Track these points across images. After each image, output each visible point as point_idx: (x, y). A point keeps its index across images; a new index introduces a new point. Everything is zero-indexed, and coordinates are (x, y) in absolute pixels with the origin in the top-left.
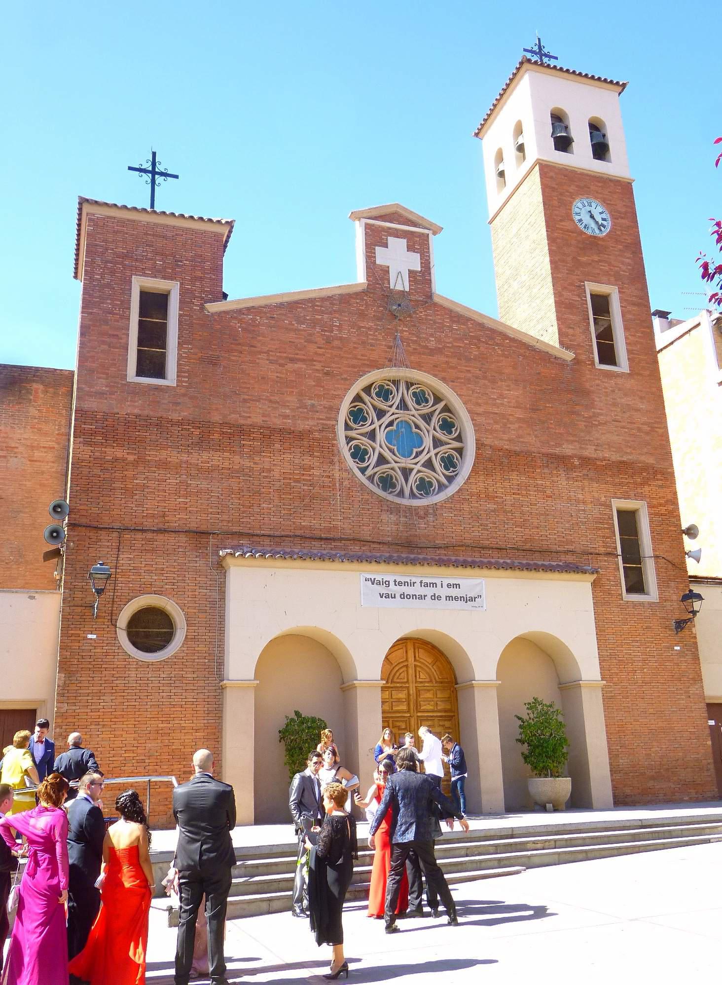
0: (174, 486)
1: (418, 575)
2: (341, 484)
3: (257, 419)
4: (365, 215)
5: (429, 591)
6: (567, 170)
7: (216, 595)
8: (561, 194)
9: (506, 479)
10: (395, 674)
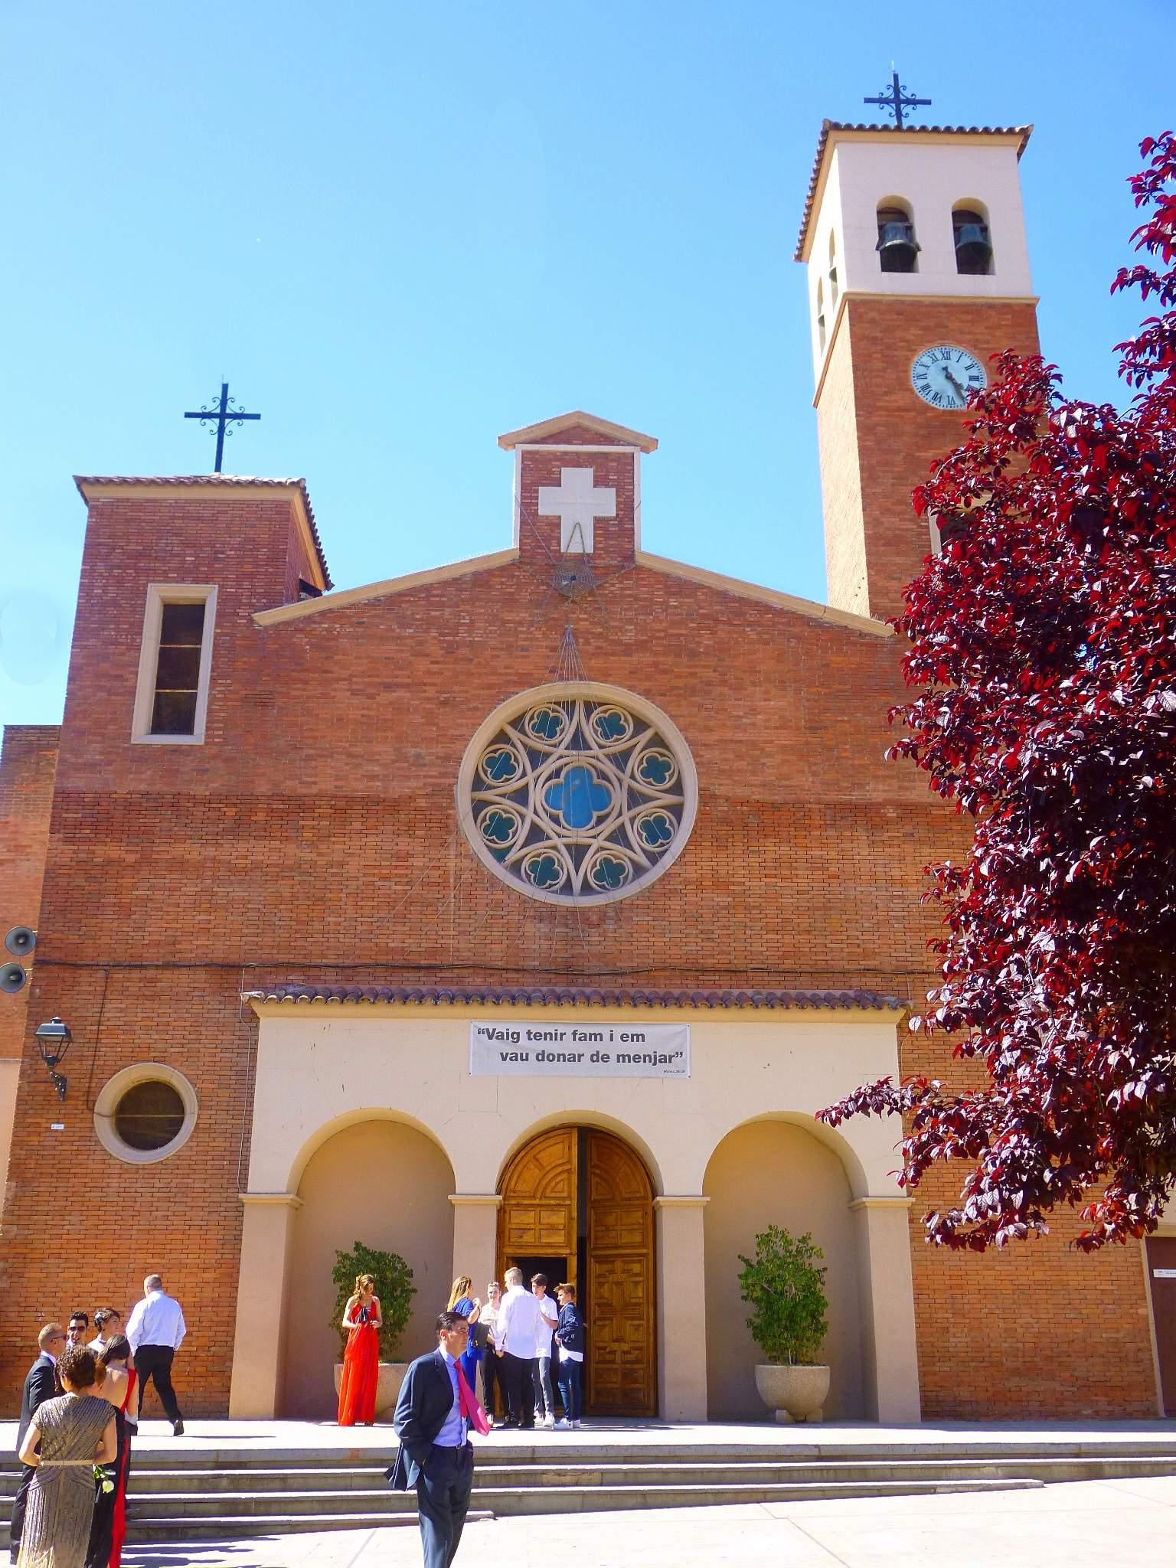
0: (190, 898)
1: (565, 1020)
2: (458, 878)
3: (327, 785)
4: (524, 438)
5: (588, 1048)
6: (903, 302)
7: (245, 1061)
8: (889, 347)
9: (753, 852)
10: (545, 1188)
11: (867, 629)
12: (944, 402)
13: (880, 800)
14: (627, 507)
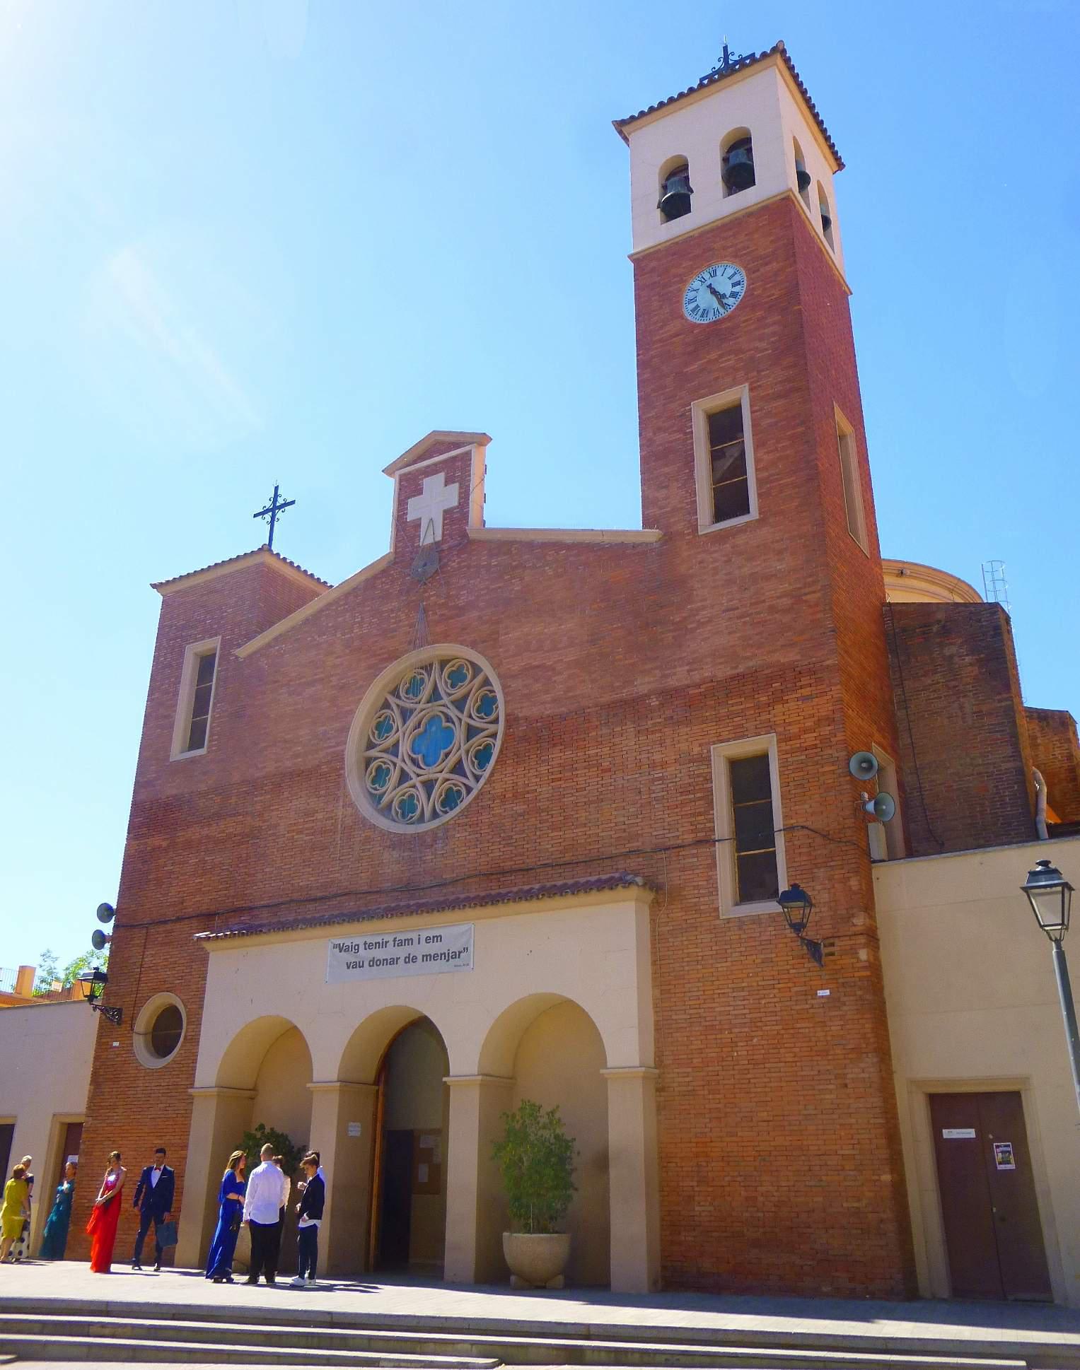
5: (402, 952)
12: (711, 315)
14: (465, 495)
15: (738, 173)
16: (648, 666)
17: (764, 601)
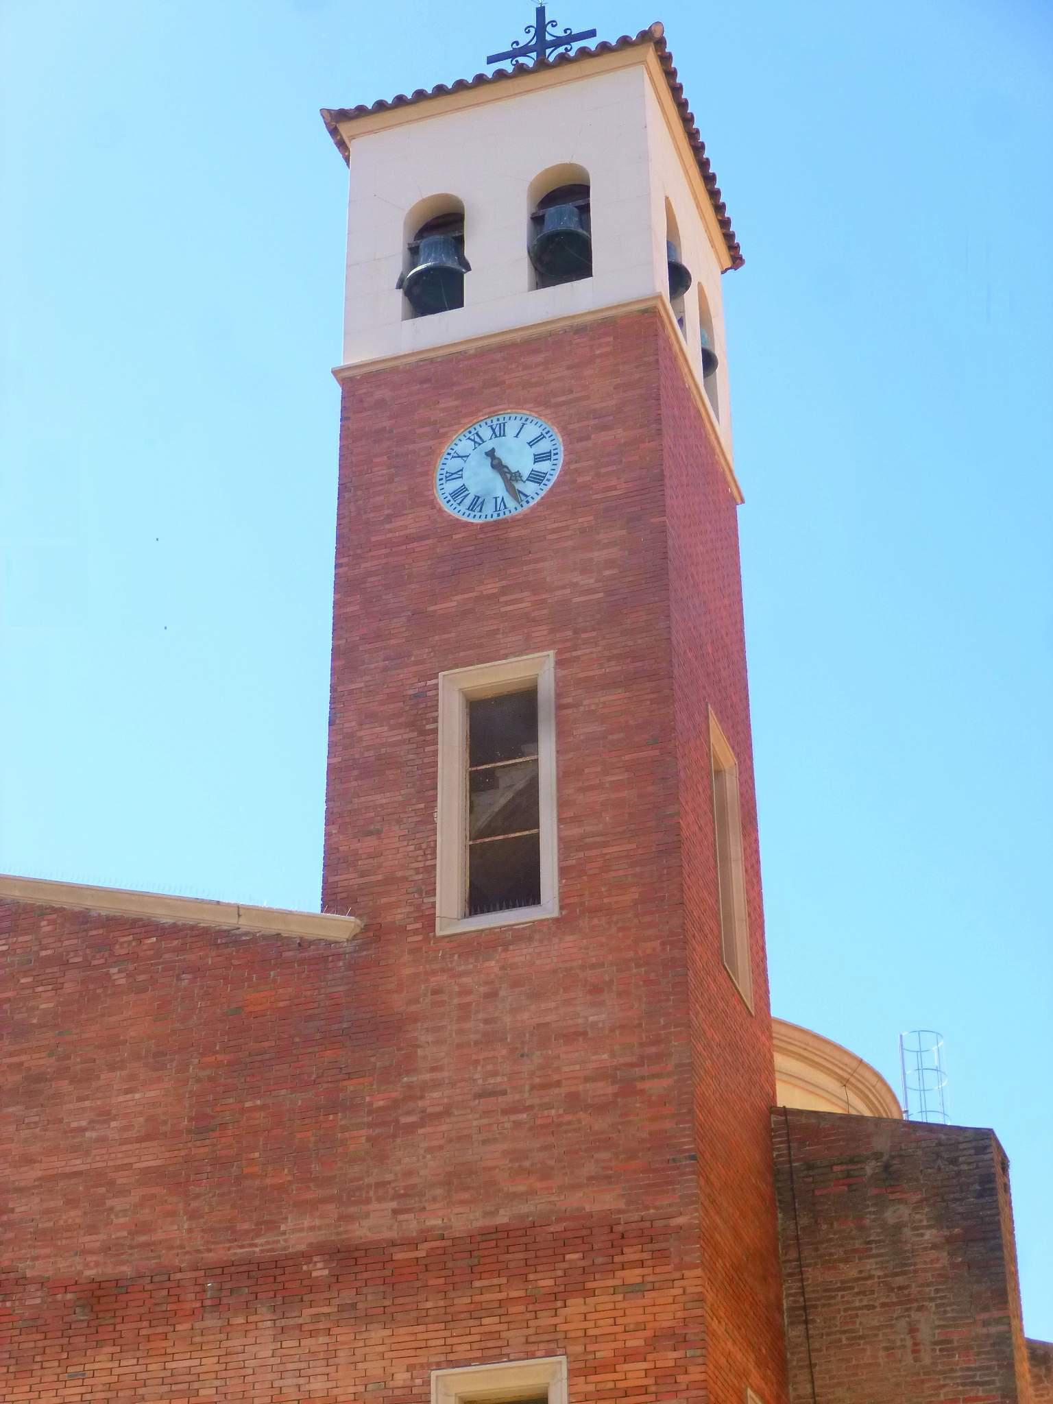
11: (312, 933)
12: (489, 509)
13: (302, 1247)
15: (561, 249)
16: (313, 1193)
17: (558, 1084)
